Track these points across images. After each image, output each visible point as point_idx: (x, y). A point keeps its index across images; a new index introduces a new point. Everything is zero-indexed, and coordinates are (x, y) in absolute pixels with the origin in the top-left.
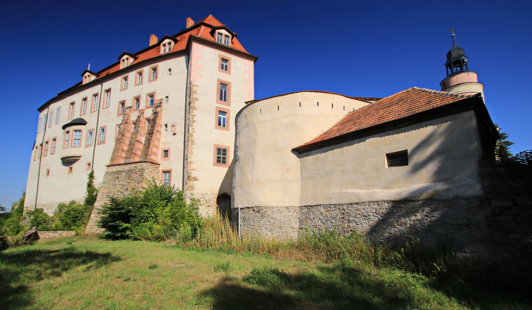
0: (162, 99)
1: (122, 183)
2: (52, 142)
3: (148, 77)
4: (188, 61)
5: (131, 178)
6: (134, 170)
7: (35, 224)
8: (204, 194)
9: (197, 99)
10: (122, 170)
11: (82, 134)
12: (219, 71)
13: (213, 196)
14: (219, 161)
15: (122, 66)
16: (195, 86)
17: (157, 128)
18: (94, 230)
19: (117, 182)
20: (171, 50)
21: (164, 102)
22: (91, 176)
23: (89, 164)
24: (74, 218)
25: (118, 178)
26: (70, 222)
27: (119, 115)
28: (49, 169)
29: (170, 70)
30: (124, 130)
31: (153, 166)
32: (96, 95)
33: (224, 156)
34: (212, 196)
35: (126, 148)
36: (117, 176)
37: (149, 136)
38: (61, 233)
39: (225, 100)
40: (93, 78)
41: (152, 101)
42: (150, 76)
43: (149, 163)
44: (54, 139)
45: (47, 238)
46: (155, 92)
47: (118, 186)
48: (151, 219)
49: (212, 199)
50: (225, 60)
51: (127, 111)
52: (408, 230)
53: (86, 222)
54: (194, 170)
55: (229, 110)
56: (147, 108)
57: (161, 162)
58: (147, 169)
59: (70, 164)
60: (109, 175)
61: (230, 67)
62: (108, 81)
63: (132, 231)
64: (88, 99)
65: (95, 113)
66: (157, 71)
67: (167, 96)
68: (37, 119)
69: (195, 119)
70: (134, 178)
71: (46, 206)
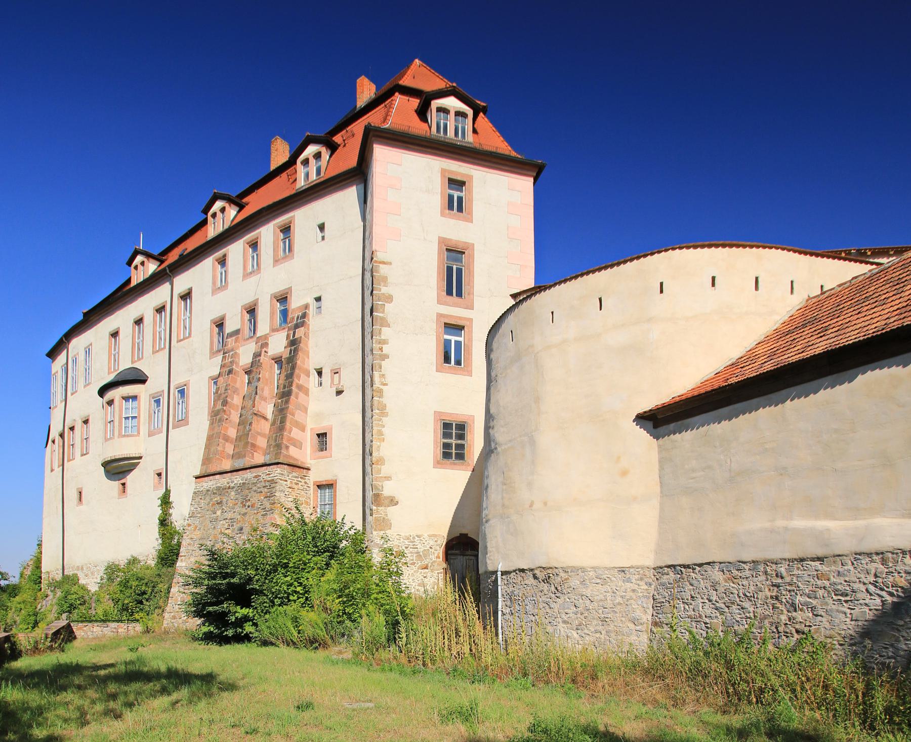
0: (307, 306)
1: (229, 515)
2: (82, 427)
3: (271, 252)
4: (364, 199)
5: (247, 504)
6: (254, 483)
7: (65, 607)
8: (414, 538)
9: (389, 299)
10: (228, 485)
11: (139, 404)
12: (442, 214)
13: (436, 541)
14: (446, 455)
15: (213, 230)
16: (384, 263)
17: (300, 380)
18: (180, 621)
19: (219, 513)
20: (322, 174)
21: (311, 312)
22: (166, 501)
23: (159, 475)
24: (139, 595)
25: (219, 503)
26: (131, 604)
27: (213, 354)
28: (82, 488)
29: (322, 227)
30: (226, 390)
31: (294, 474)
32: (160, 310)
33: (459, 442)
34: (432, 543)
35: (232, 433)
36: (218, 498)
37: (282, 401)
38: (115, 628)
39: (459, 294)
40: (152, 267)
41: (284, 313)
42: (275, 250)
43: (286, 466)
44: (84, 420)
45: (91, 637)
46: (290, 289)
47: (221, 522)
48: (295, 598)
49: (433, 550)
50: (456, 183)
51: (231, 342)
53: (162, 605)
54: (388, 478)
55: (471, 320)
56: (274, 330)
57: (313, 462)
58: (281, 480)
59: (121, 476)
60: (201, 499)
61: (471, 201)
62: (180, 274)
63: (255, 625)
64: (146, 321)
65: (161, 353)
67: (317, 295)
68: (48, 377)
69: (386, 349)
70: (254, 504)
71: (82, 569)
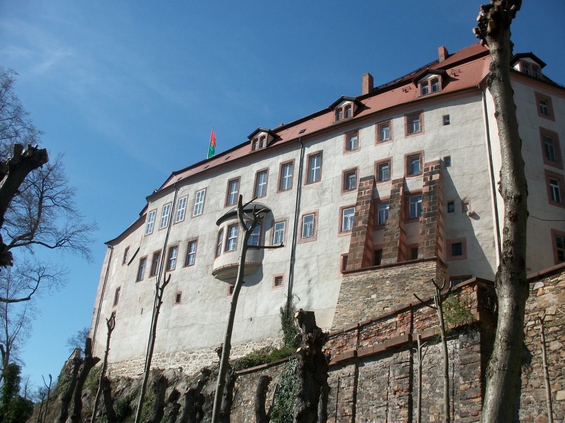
37: (429, 220)
52: (121, 399)
66: (421, 121)
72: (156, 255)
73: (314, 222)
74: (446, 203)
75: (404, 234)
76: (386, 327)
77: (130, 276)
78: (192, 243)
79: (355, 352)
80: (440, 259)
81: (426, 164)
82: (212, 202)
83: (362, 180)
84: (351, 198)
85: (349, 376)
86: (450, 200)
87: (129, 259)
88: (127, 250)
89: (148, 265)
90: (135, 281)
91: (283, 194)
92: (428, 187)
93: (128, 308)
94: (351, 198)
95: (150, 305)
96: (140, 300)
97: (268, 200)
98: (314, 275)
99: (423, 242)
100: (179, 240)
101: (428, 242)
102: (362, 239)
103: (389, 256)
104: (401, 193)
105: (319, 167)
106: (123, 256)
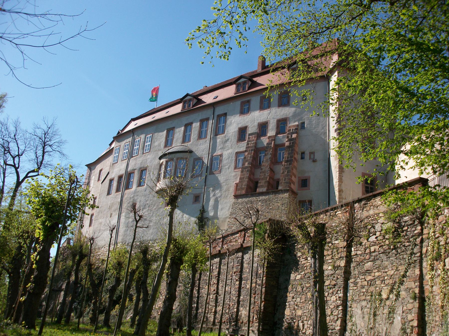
33: (372, 186)
37: (287, 164)
72: (120, 177)
73: (220, 161)
74: (300, 153)
75: (272, 172)
76: (234, 239)
77: (103, 191)
78: (143, 171)
79: (220, 251)
80: (292, 189)
81: (290, 127)
82: (156, 144)
83: (250, 135)
84: (243, 146)
85: (217, 263)
86: (302, 151)
87: (102, 178)
88: (101, 171)
89: (115, 184)
90: (106, 194)
91: (201, 141)
92: (289, 142)
93: (101, 213)
94: (243, 146)
95: (116, 212)
96: (110, 208)
97: (191, 144)
98: (218, 196)
99: (283, 179)
100: (134, 168)
101: (286, 179)
102: (247, 175)
103: (262, 186)
104: (272, 145)
105: (224, 124)
106: (98, 175)
